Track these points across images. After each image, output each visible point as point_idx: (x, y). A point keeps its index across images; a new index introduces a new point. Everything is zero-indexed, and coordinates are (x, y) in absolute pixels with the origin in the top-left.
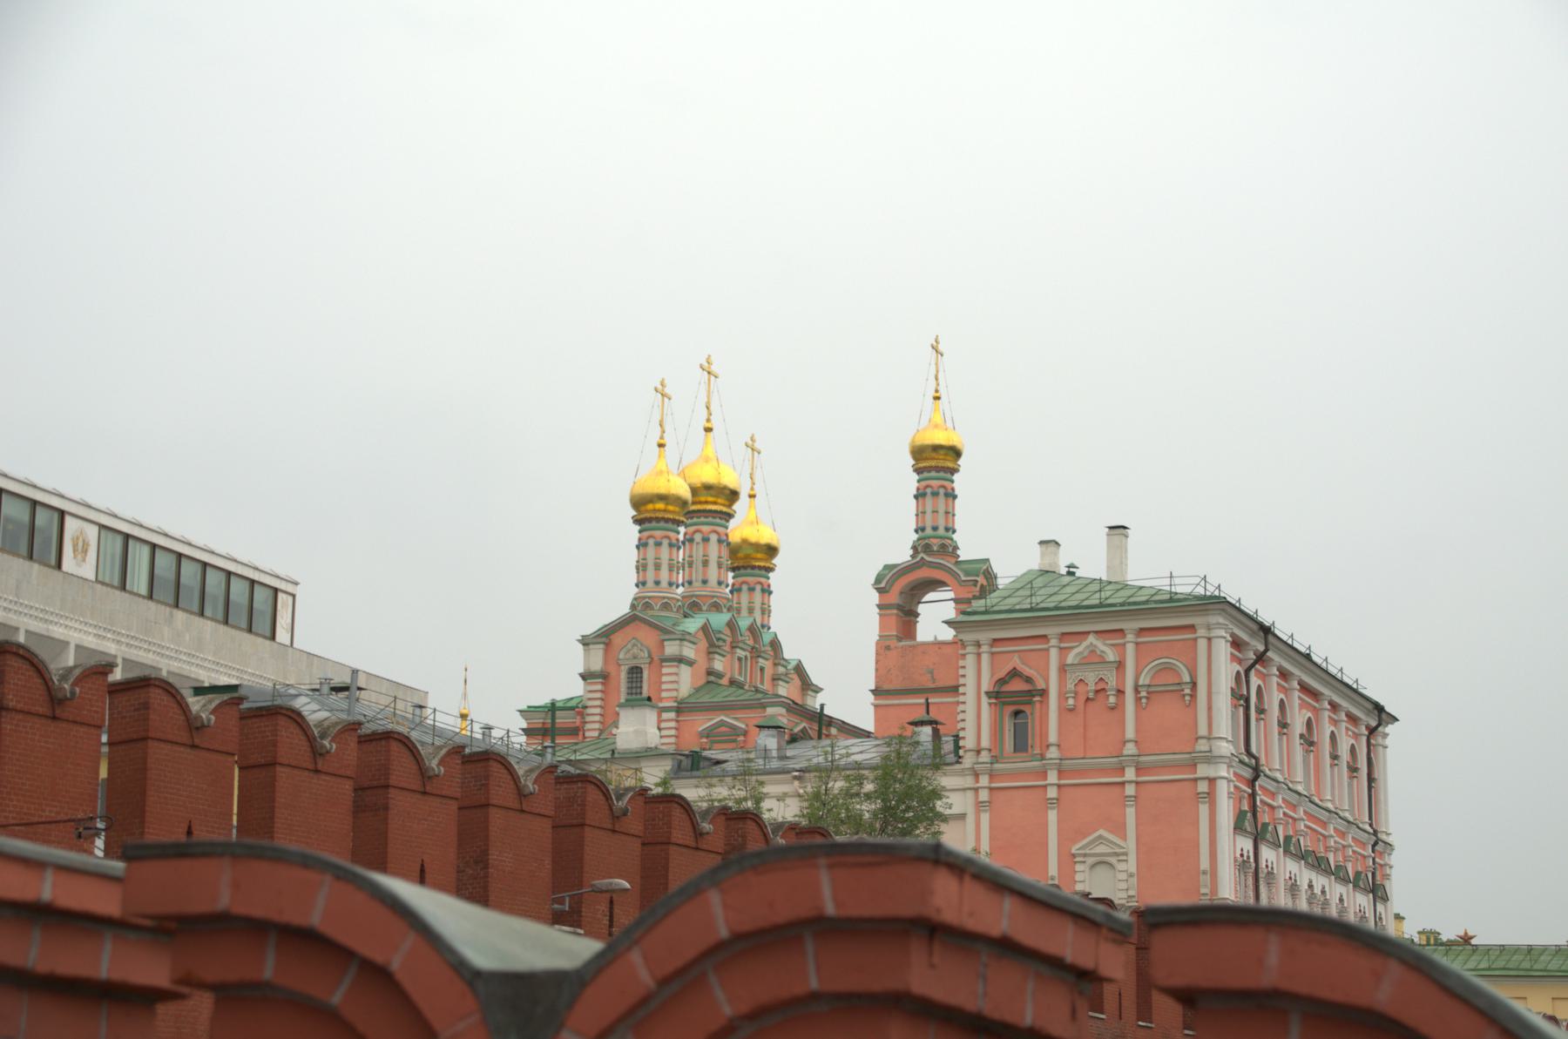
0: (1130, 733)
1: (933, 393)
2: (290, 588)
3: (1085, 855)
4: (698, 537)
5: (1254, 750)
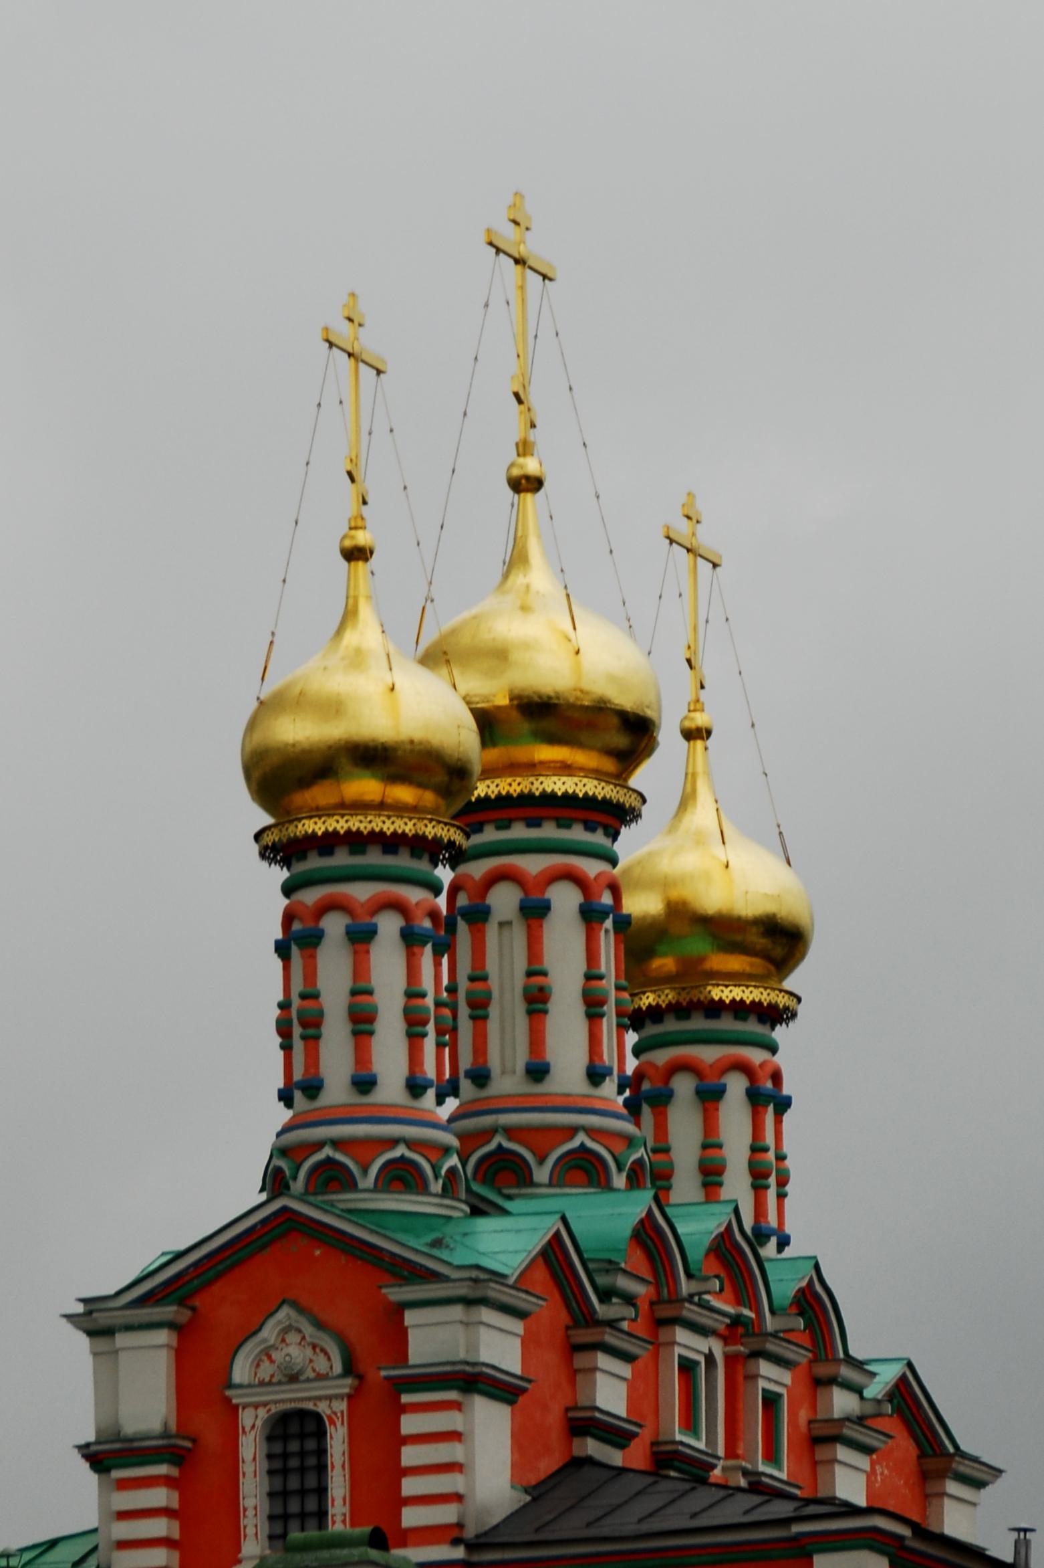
4: (505, 900)
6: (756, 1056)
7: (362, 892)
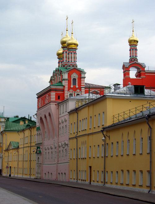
7: (71, 51)
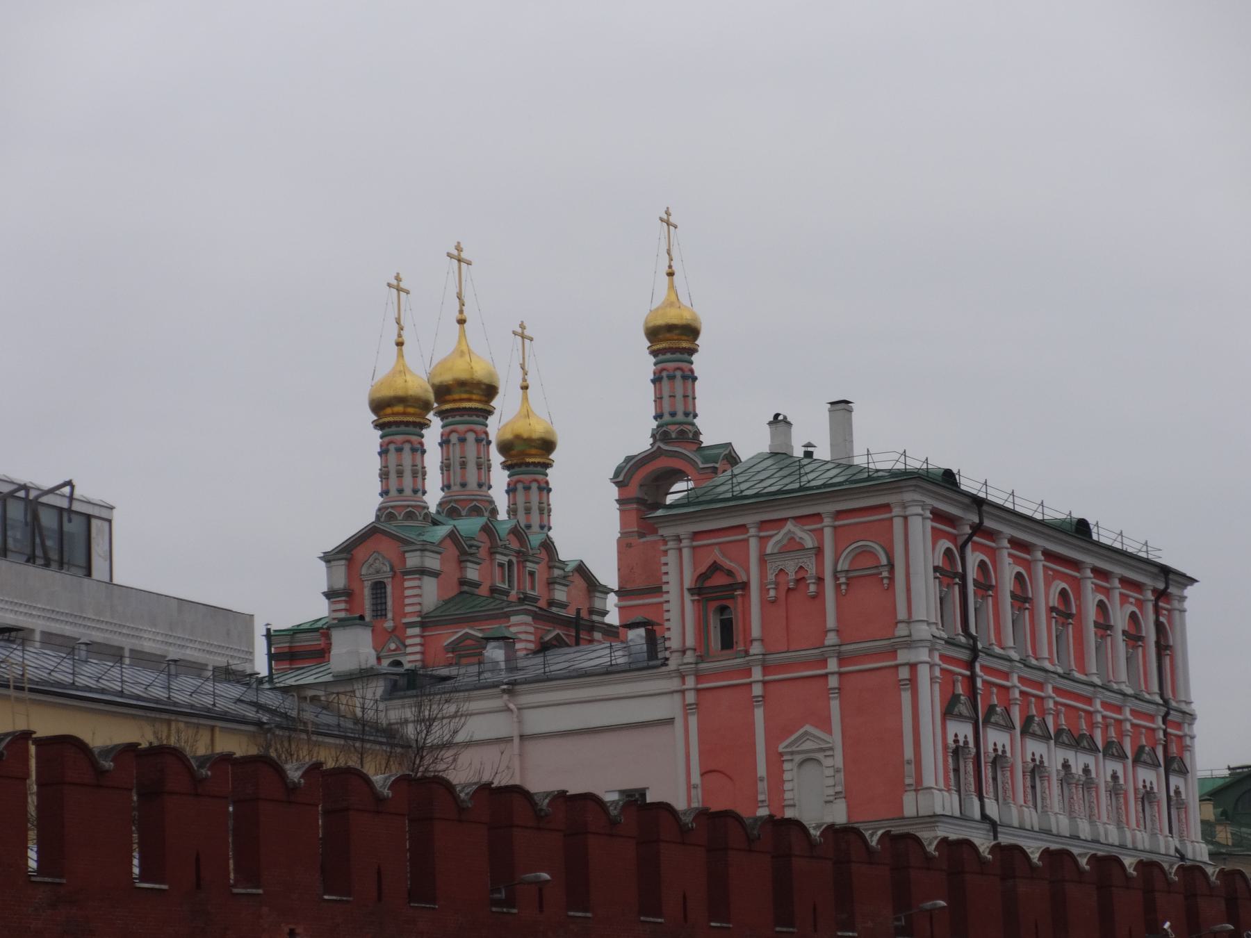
0: (831, 622)
1: (666, 269)
2: (104, 513)
3: (792, 753)
5: (973, 631)
6: (540, 477)
